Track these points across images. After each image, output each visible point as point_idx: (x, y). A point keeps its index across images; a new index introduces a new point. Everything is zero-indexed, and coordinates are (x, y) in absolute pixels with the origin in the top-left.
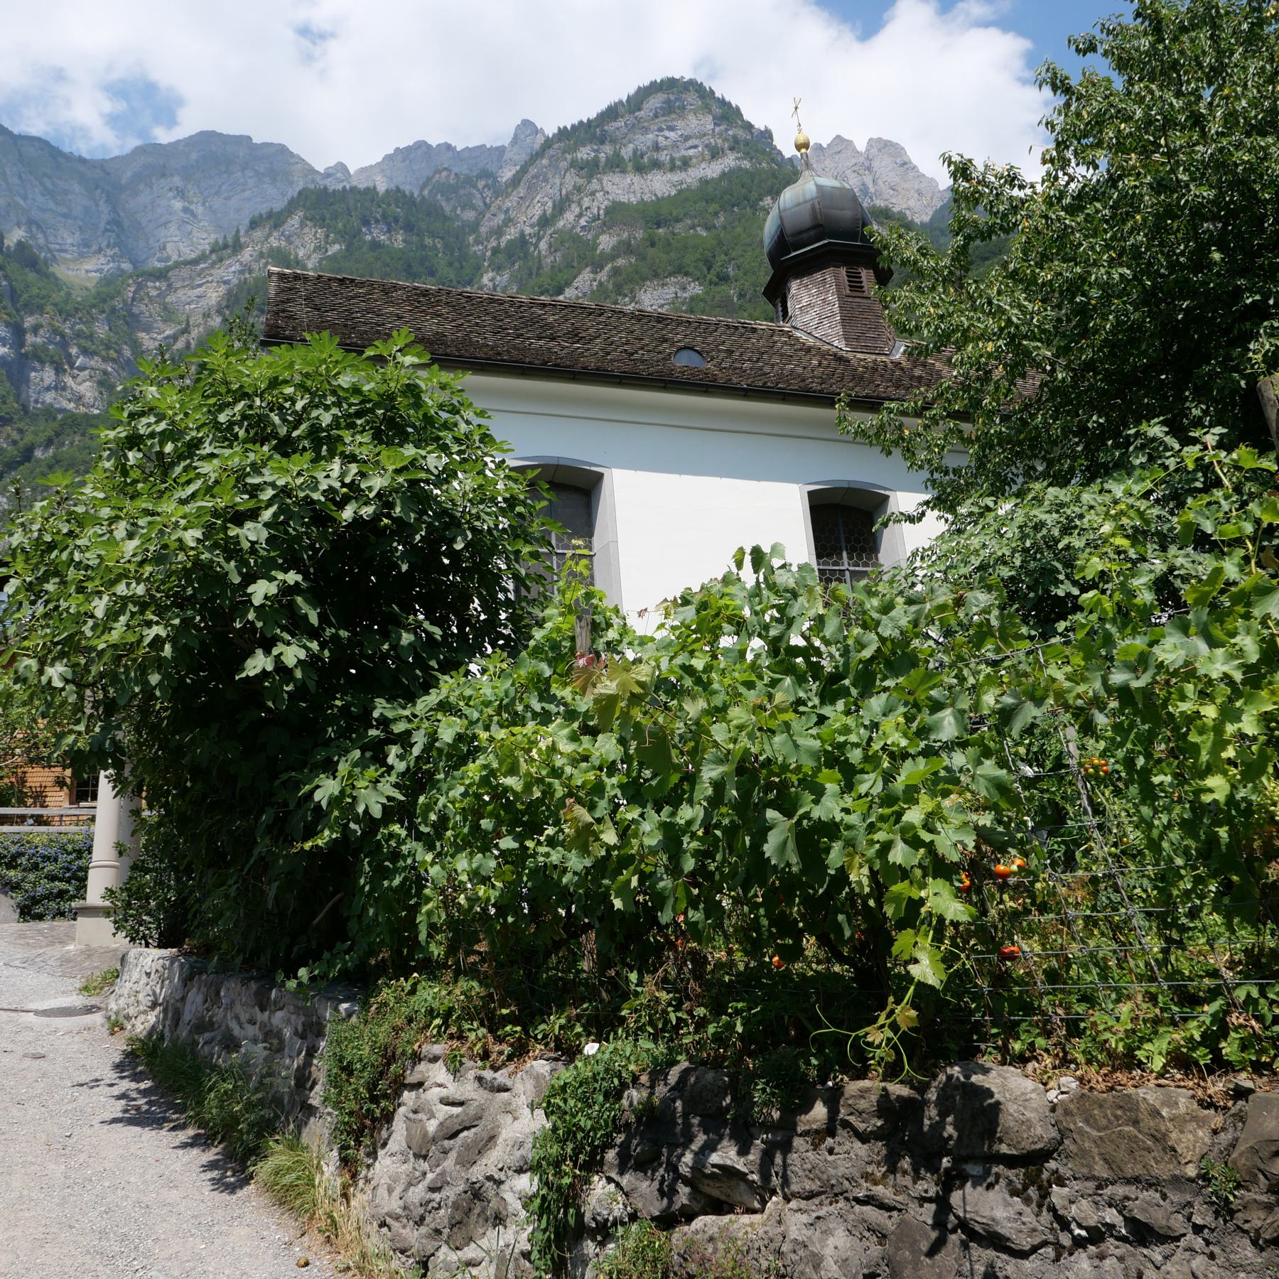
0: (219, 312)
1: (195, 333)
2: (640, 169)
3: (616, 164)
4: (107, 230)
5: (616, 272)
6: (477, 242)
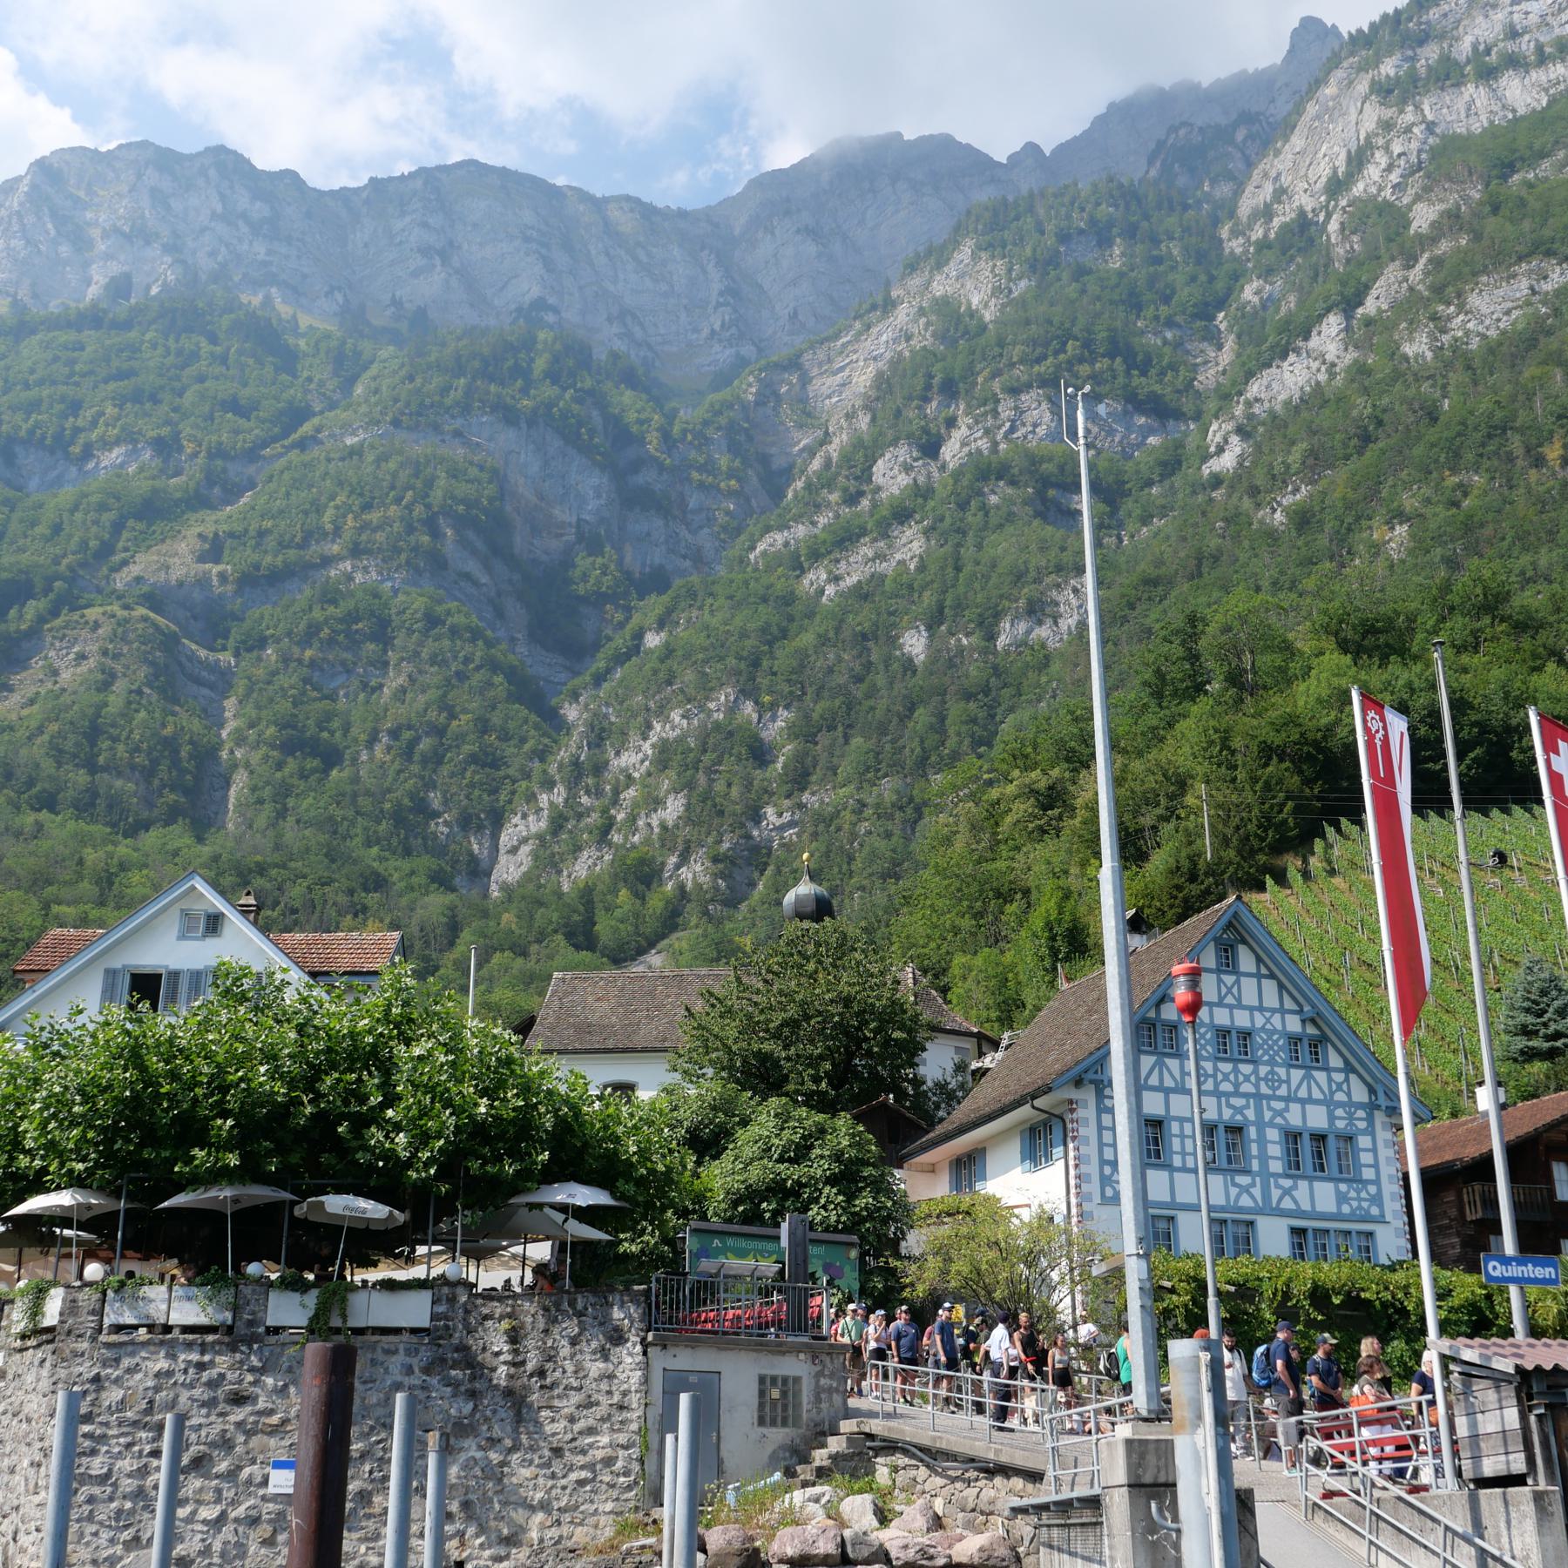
0: (866, 407)
1: (834, 449)
2: (1487, 74)
3: (1448, 75)
4: (719, 305)
5: (1437, 262)
6: (1235, 233)
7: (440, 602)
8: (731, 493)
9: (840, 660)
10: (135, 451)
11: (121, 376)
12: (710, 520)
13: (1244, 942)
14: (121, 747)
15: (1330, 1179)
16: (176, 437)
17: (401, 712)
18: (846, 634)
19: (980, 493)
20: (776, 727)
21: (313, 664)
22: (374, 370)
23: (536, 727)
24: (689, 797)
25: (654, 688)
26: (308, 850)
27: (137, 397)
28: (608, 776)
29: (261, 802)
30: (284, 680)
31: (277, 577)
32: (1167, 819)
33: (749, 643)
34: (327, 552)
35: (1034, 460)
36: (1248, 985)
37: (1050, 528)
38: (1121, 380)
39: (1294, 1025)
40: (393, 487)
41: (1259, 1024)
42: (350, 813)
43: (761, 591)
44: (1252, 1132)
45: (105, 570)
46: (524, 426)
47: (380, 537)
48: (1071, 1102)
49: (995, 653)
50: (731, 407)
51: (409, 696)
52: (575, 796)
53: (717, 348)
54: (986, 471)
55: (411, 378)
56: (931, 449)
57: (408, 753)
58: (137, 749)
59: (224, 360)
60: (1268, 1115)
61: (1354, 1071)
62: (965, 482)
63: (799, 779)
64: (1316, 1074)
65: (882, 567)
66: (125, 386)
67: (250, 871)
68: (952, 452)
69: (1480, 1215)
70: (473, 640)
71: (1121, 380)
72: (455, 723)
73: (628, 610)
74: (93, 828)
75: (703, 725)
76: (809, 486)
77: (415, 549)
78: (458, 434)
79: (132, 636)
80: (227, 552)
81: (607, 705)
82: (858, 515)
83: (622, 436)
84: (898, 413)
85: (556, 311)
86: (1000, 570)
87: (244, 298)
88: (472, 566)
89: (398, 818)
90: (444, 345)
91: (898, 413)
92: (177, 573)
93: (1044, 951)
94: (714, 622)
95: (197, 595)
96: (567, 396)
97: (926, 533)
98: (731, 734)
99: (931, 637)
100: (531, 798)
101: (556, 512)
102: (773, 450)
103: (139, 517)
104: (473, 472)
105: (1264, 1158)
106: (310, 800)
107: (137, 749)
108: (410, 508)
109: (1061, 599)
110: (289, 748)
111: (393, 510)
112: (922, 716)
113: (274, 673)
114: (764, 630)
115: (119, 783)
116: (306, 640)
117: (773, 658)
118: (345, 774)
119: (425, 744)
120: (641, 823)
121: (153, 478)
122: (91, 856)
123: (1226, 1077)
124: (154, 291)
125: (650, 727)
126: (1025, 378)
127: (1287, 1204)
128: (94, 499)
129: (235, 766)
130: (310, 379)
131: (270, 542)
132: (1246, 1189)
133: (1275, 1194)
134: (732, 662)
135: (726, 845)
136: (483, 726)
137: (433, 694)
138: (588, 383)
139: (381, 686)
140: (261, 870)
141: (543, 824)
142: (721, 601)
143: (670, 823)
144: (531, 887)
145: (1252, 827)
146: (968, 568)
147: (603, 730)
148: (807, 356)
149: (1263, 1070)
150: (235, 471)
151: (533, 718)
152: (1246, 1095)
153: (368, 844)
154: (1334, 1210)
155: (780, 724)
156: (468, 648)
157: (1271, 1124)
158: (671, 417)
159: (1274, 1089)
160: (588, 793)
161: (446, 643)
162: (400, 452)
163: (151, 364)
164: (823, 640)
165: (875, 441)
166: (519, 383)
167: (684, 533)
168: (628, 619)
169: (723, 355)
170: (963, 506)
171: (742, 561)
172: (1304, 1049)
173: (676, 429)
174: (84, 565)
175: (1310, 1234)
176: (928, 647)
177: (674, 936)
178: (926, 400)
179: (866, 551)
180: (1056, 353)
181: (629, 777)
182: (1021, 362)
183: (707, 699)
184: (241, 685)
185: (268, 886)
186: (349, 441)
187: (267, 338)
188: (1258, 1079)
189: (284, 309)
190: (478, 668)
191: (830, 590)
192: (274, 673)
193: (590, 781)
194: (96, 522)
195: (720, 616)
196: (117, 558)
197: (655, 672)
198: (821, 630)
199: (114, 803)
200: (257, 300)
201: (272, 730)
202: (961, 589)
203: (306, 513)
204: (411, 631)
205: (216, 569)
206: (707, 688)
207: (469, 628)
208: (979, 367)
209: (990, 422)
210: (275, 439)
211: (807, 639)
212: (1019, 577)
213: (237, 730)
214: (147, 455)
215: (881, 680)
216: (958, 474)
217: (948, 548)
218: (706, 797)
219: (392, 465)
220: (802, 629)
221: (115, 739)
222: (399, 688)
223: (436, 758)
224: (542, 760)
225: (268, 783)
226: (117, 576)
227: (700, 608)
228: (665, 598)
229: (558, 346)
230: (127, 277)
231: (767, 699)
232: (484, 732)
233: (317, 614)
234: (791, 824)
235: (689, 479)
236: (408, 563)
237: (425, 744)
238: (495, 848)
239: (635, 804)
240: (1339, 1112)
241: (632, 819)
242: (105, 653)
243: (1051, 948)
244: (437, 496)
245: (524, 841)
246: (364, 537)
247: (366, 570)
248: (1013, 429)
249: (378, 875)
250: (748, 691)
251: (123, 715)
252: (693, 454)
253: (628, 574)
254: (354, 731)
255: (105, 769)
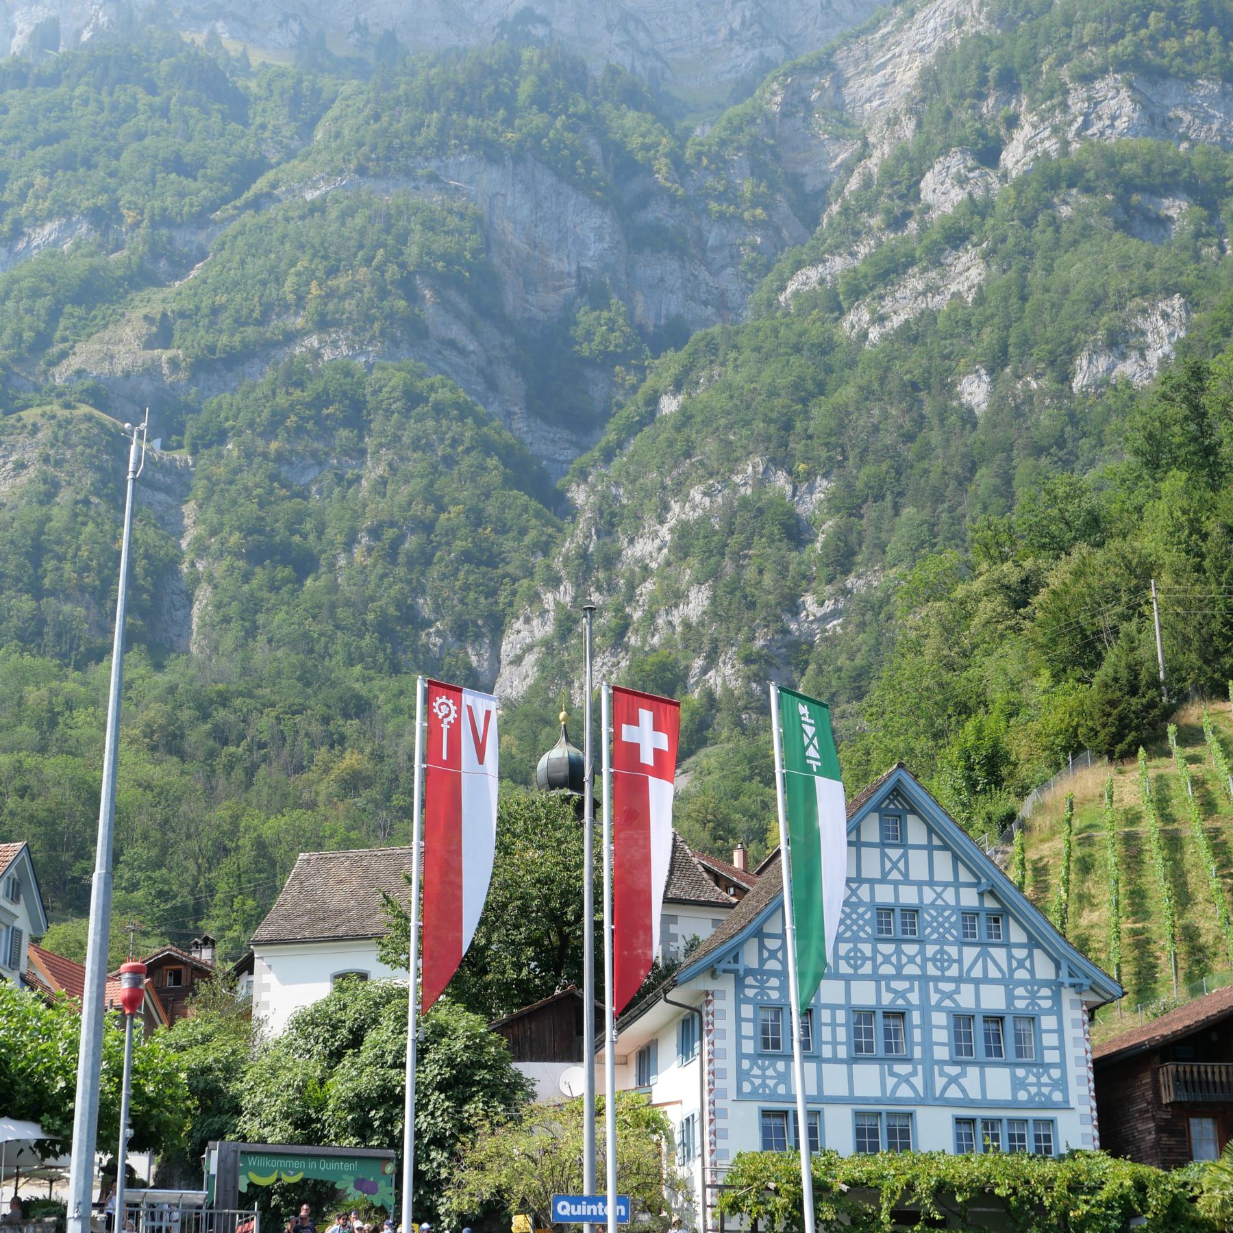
0: (910, 111)
1: (873, 164)
7: (421, 376)
8: (756, 224)
9: (886, 416)
10: (69, 225)
11: (49, 140)
12: (734, 258)
13: (913, 811)
14: (68, 567)
15: (1005, 1065)
16: (114, 205)
17: (380, 508)
18: (893, 385)
19: (1049, 205)
20: (814, 501)
21: (280, 458)
22: (334, 111)
23: (538, 515)
24: (714, 589)
25: (670, 462)
26: (279, 673)
27: (68, 163)
28: (621, 568)
29: (227, 620)
30: (248, 479)
31: (234, 360)
32: (1128, 618)
33: (778, 402)
34: (290, 327)
35: (1112, 160)
36: (918, 860)
37: (1134, 242)
38: (1217, 55)
39: (970, 898)
40: (361, 247)
41: (927, 901)
42: (329, 628)
43: (793, 339)
44: (916, 1018)
45: (42, 365)
46: (509, 163)
47: (349, 305)
48: (707, 993)
49: (1071, 396)
50: (752, 121)
51: (390, 488)
52: (586, 593)
53: (738, 50)
54: (1054, 178)
55: (377, 117)
56: (989, 155)
57: (392, 554)
58: (87, 568)
59: (164, 112)
60: (934, 998)
61: (1039, 946)
62: (1030, 193)
63: (843, 560)
64: (994, 951)
65: (934, 302)
66: (57, 149)
67: (212, 702)
68: (1014, 158)
69: (1172, 1098)
70: (461, 418)
71: (1217, 55)
72: (443, 517)
73: (642, 370)
74: (39, 662)
75: (728, 503)
76: (845, 211)
77: (390, 316)
78: (433, 178)
79: (75, 439)
80: (177, 335)
81: (617, 484)
82: (905, 241)
83: (627, 166)
84: (948, 116)
85: (545, 21)
86: (1074, 296)
87: (186, 37)
88: (457, 332)
89: (384, 631)
90: (413, 74)
91: (948, 116)
92: (123, 362)
93: (961, 783)
94: (738, 379)
95: (146, 387)
96: (558, 124)
97: (987, 256)
98: (760, 511)
99: (993, 382)
100: (535, 598)
101: (552, 261)
102: (806, 169)
103: (77, 301)
104: (453, 221)
105: (928, 1045)
106: (282, 615)
107: (87, 568)
108: (381, 269)
109: (1148, 326)
110: (256, 556)
111: (363, 273)
112: (985, 478)
113: (236, 471)
114: (797, 386)
115: (67, 608)
116: (270, 432)
117: (809, 419)
118: (322, 582)
119: (411, 543)
120: (660, 621)
121: (91, 255)
122: (34, 695)
123: (887, 959)
124: (86, 36)
125: (666, 508)
126: (1099, 61)
127: (954, 1092)
128: (25, 284)
129: (197, 581)
130: (263, 127)
131: (225, 320)
132: (906, 1079)
133: (940, 1082)
134: (759, 426)
135: (759, 643)
136: (477, 518)
137: (417, 484)
138: (582, 107)
139: (358, 479)
140: (224, 700)
141: (550, 629)
142: (747, 353)
143: (694, 620)
144: (537, 703)
145: (1216, 626)
146: (1037, 296)
147: (613, 514)
148: (841, 54)
149: (931, 950)
150: (183, 240)
151: (534, 504)
152: (910, 978)
153: (350, 662)
154: (1009, 1098)
155: (819, 496)
156: (456, 428)
157: (938, 1008)
158: (682, 138)
159: (943, 970)
160: (599, 589)
161: (430, 424)
162: (368, 205)
163: (83, 123)
164: (867, 394)
165: (922, 151)
166: (502, 113)
167: (704, 275)
168: (643, 380)
169: (745, 58)
170: (1029, 222)
171: (771, 304)
172: (981, 925)
173: (689, 153)
174: (19, 360)
175: (979, 1125)
176: (991, 394)
177: (702, 752)
178: (981, 96)
179: (915, 282)
180: (1136, 28)
181: (646, 568)
182: (1094, 42)
183: (732, 471)
184: (200, 487)
185: (232, 718)
186: (310, 195)
187: (213, 84)
188: (925, 960)
189: (233, 47)
190: (468, 451)
191: (874, 334)
192: (236, 471)
193: (601, 575)
194: (29, 311)
195: (744, 373)
196: (55, 350)
197: (671, 443)
198: (863, 382)
199: (64, 631)
200: (200, 38)
201: (235, 538)
202: (1027, 323)
203: (264, 283)
204: (388, 413)
205: (166, 355)
206: (731, 459)
207: (456, 405)
208: (1043, 52)
209: (1059, 117)
210: (225, 200)
211: (847, 394)
212: (1096, 303)
213: (198, 539)
214: (83, 228)
215: (935, 437)
216: (1021, 184)
217: (1012, 274)
218: (733, 589)
219: (359, 220)
220: (843, 381)
221: (61, 558)
222: (378, 481)
223: (424, 559)
224: (546, 554)
225: (234, 598)
226: (56, 370)
227: (723, 364)
228: (682, 355)
229: (545, 66)
230: (54, 23)
231: (802, 467)
232: (478, 525)
233: (281, 400)
234: (835, 614)
235: (706, 211)
236: (382, 333)
237: (411, 543)
238: (496, 659)
239: (654, 601)
240: (1020, 991)
241: (651, 617)
242: (46, 460)
243: (969, 779)
244: (412, 252)
245: (529, 648)
246: (331, 307)
247: (335, 345)
248: (1086, 125)
249: (358, 697)
250: (780, 460)
251: (68, 530)
252: (710, 181)
253: (640, 329)
254: (330, 532)
255: (52, 593)
